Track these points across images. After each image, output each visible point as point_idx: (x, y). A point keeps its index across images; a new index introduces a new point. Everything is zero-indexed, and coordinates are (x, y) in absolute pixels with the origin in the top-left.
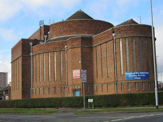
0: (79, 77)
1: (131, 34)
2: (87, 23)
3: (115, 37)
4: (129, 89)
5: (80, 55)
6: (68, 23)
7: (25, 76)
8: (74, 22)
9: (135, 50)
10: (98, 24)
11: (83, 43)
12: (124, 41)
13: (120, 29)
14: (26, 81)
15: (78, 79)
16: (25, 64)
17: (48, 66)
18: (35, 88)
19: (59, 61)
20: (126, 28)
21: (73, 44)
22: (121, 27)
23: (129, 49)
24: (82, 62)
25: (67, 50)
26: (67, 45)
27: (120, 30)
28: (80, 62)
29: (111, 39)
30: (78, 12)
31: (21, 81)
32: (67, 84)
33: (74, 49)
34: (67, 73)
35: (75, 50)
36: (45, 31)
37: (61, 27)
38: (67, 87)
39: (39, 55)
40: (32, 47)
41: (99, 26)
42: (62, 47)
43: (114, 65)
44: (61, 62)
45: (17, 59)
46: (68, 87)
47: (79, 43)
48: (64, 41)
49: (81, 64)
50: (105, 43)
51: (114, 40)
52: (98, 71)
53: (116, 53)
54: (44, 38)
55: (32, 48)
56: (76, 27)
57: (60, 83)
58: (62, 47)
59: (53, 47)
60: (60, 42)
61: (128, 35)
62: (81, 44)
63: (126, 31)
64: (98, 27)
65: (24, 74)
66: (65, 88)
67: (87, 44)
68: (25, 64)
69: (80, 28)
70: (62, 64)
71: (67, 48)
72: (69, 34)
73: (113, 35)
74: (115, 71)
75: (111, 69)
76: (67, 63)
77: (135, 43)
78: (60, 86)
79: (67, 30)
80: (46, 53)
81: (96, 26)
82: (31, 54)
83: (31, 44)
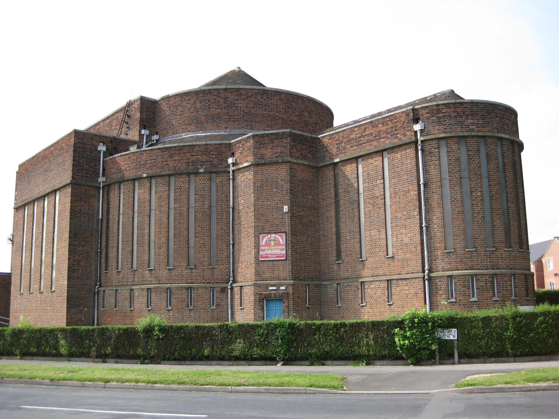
0: (281, 257)
1: (474, 127)
2: (280, 100)
3: (421, 136)
4: (473, 296)
5: (287, 186)
6: (222, 95)
7: (78, 248)
8: (240, 95)
9: (215, 205)
10: (307, 107)
11: (294, 151)
12: (164, 188)
13: (439, 111)
14: (82, 263)
15: (276, 263)
16: (80, 210)
17: (165, 220)
18: (114, 289)
19: (207, 203)
20: (460, 110)
21: (263, 151)
22: (444, 104)
23: (470, 171)
24: (291, 209)
25: (233, 171)
26: (233, 155)
27: (440, 115)
28: (286, 209)
29: (405, 140)
30: (233, 73)
31: (67, 265)
32: (231, 279)
33: (266, 167)
34: (233, 244)
35: (269, 171)
36: (145, 114)
37: (198, 105)
38: (232, 289)
39: (131, 182)
40: (103, 158)
41: (309, 114)
42: (215, 162)
43: (417, 221)
44: (214, 209)
45: (43, 197)
46: (237, 290)
47: (283, 149)
48: (223, 142)
49: (290, 215)
50: (376, 152)
51: (419, 142)
52: (342, 239)
53: (425, 185)
54: (141, 136)
55: (103, 162)
56: (247, 107)
57: (208, 274)
58: (215, 162)
59: (185, 161)
60: (211, 145)
61: (468, 129)
62: (291, 152)
63: (459, 119)
64: (306, 114)
65: (77, 243)
66: (224, 290)
67: (304, 157)
68: (80, 210)
69: (260, 112)
70: (214, 216)
71: (234, 164)
72: (226, 128)
73: (417, 127)
74: (422, 240)
75: (404, 232)
76: (233, 211)
77: (488, 155)
78: (209, 285)
79: (219, 116)
80: (159, 180)
81: (302, 111)
82: (101, 179)
83: (102, 148)
